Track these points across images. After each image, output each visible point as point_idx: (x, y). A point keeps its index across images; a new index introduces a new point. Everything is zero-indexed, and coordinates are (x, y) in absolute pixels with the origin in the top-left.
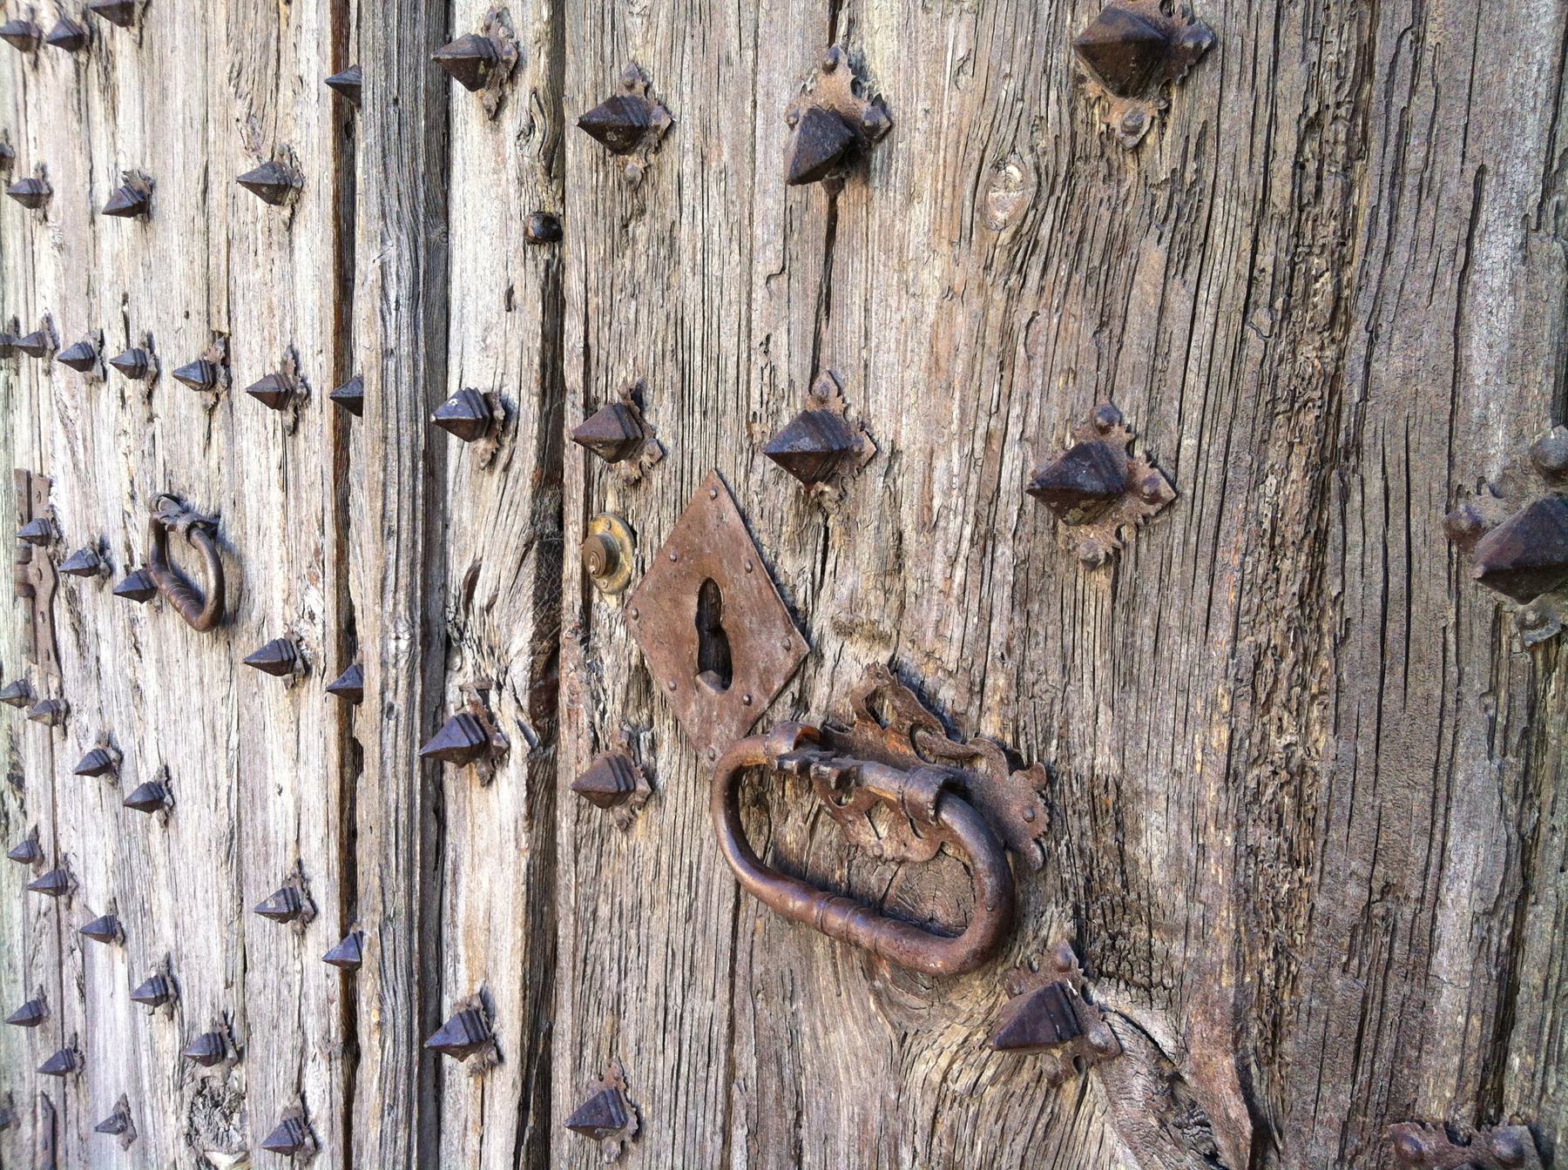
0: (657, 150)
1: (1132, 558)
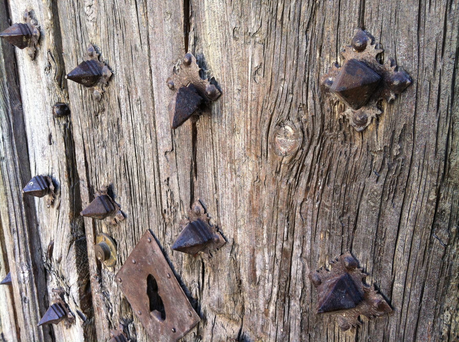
0: (107, 86)
1: (366, 330)
